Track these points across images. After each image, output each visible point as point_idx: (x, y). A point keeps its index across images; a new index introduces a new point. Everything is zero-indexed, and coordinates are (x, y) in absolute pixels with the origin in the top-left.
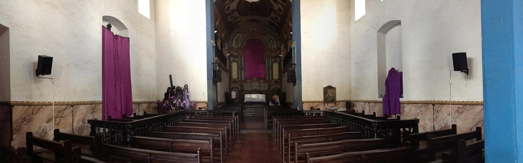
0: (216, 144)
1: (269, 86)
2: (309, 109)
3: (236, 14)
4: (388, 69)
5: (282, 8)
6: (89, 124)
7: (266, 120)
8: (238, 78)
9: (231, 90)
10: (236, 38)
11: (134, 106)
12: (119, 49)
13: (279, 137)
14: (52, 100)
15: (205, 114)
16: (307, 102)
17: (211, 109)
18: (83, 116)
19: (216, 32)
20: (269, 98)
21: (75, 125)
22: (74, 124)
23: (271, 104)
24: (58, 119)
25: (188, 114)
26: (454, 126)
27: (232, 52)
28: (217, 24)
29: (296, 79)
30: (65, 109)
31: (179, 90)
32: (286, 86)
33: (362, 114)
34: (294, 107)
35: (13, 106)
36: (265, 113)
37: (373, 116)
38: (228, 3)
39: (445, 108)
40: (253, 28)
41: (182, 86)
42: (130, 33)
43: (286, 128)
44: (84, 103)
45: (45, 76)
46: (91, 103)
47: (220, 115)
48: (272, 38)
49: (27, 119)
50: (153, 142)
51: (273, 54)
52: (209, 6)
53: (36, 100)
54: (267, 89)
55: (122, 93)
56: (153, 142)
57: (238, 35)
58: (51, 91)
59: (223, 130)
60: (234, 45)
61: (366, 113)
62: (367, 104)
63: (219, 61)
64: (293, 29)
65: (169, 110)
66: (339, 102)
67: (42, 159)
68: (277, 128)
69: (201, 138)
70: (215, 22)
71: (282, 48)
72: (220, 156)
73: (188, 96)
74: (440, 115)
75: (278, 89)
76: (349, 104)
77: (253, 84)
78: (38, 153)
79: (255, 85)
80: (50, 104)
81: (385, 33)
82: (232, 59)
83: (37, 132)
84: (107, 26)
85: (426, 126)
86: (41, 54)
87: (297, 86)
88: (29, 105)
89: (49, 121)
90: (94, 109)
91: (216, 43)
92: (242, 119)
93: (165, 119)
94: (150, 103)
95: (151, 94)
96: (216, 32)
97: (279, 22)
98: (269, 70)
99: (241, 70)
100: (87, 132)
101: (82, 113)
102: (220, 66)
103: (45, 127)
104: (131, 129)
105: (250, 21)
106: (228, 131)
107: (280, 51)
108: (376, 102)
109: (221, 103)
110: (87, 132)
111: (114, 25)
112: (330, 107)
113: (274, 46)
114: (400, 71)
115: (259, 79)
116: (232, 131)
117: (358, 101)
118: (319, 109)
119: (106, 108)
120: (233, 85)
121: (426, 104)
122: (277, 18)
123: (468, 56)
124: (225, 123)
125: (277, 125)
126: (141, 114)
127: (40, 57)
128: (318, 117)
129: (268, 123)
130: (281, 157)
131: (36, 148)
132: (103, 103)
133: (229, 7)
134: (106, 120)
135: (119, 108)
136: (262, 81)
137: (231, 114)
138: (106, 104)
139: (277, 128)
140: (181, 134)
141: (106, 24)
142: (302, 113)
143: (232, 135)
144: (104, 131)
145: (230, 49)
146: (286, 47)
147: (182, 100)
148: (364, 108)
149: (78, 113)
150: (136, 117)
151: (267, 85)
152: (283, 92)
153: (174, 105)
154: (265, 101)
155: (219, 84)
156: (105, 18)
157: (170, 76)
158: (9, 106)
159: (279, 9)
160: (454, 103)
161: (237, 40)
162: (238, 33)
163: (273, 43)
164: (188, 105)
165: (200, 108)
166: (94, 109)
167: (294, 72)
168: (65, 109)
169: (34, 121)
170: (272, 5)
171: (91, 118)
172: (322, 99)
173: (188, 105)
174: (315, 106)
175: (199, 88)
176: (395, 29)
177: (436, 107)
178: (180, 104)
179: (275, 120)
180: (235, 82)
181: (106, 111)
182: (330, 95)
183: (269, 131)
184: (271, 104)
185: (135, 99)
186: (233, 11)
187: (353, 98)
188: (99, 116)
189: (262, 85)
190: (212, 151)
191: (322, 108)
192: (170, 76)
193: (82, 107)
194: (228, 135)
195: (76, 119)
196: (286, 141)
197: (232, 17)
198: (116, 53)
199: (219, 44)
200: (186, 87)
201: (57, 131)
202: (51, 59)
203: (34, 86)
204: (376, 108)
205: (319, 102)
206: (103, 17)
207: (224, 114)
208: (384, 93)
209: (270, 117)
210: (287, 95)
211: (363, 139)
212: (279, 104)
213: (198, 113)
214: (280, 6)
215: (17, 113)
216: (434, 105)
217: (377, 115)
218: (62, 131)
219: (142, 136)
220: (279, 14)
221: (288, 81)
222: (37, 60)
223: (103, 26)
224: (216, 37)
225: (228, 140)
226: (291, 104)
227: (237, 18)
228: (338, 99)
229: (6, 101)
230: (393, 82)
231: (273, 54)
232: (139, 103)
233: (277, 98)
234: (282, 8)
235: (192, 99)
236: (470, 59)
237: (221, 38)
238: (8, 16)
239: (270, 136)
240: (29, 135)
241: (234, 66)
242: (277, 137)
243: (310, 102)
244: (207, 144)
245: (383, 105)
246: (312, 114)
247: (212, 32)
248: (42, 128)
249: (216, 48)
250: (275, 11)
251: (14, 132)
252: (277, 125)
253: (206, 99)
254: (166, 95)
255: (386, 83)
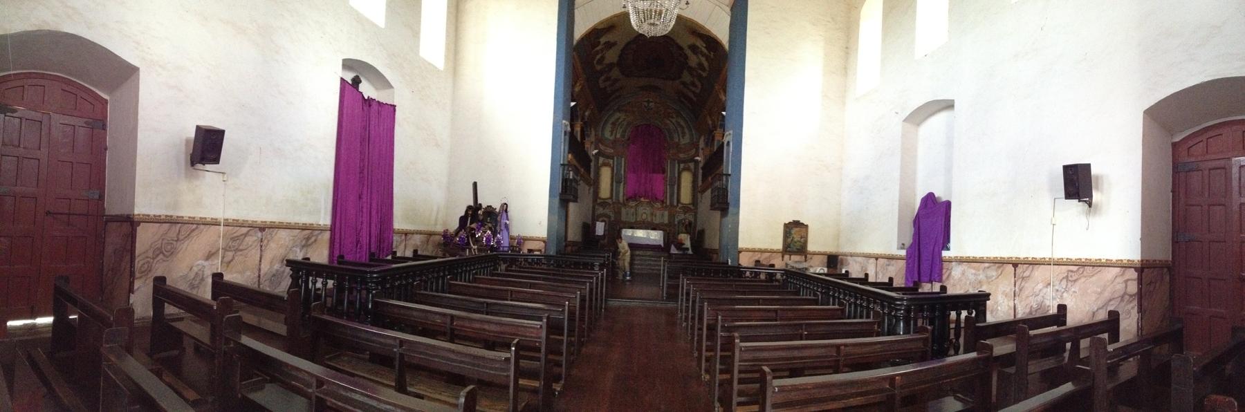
0: (554, 327)
1: (672, 216)
2: (752, 265)
3: (615, 73)
4: (921, 194)
5: (706, 64)
6: (288, 269)
7: (665, 281)
8: (611, 197)
9: (595, 219)
10: (612, 120)
11: (396, 238)
12: (372, 127)
13: (693, 318)
14: (219, 214)
15: (539, 262)
16: (748, 250)
17: (552, 252)
18: (282, 251)
19: (573, 104)
20: (670, 239)
21: (265, 267)
22: (258, 268)
23: (674, 250)
24: (230, 254)
25: (505, 261)
26: (1062, 308)
27: (602, 147)
28: (577, 89)
29: (728, 204)
30: (246, 235)
31: (490, 212)
32: (709, 219)
33: (864, 280)
34: (721, 259)
35: (139, 223)
36: (662, 265)
37: (889, 285)
38: (602, 50)
39: (1039, 272)
40: (648, 102)
41: (497, 206)
42: (401, 97)
43: (710, 301)
44: (288, 227)
45: (208, 167)
46: (304, 228)
47: (569, 266)
48: (682, 123)
49: (166, 251)
50: (415, 313)
51: (682, 156)
52: (563, 55)
53: (186, 212)
54: (666, 220)
55: (374, 213)
56: (415, 313)
57: (617, 115)
58: (214, 197)
59: (573, 298)
60: (607, 134)
61: (871, 279)
62: (873, 260)
63: (575, 162)
64: (729, 104)
65: (464, 250)
66: (814, 254)
67: (180, 334)
68: (688, 300)
69: (518, 312)
70: (573, 86)
71: (702, 144)
72: (539, 350)
73: (507, 226)
74: (1028, 286)
75: (690, 223)
76: (833, 260)
77: (641, 210)
78: (174, 320)
79: (644, 212)
80: (215, 223)
81: (918, 125)
82: (601, 160)
83: (184, 277)
84: (353, 80)
85: (999, 310)
86: (203, 123)
87: (729, 218)
88: (172, 221)
89: (210, 256)
90: (308, 239)
91: (572, 126)
92: (614, 281)
93: (452, 268)
94: (430, 234)
95: (433, 218)
96: (573, 104)
97: (698, 91)
98: (672, 186)
99: (619, 182)
100: (282, 287)
101: (281, 247)
102: (577, 171)
103: (192, 268)
104: (377, 284)
105: (642, 88)
106: (583, 300)
107: (697, 149)
108: (891, 258)
109: (574, 243)
110: (282, 287)
111: (368, 80)
112: (794, 261)
113: (685, 140)
114: (944, 199)
115: (653, 199)
116: (591, 300)
117: (852, 255)
118: (773, 266)
119: (337, 240)
120: (600, 211)
121: (1000, 263)
122: (693, 84)
123: (1094, 171)
124: (577, 283)
125: (688, 294)
126: (409, 254)
127: (198, 128)
128: (772, 281)
129: (669, 287)
130: (694, 364)
131: (170, 310)
132: (333, 229)
133: (603, 58)
134: (336, 264)
135: (365, 241)
136: (658, 205)
137: (593, 266)
138: (337, 230)
139: (688, 300)
140: (482, 303)
141: (349, 77)
142: (738, 271)
143: (590, 308)
144: (325, 284)
145: (599, 141)
146: (710, 140)
147: (495, 233)
148: (863, 268)
149: (273, 245)
150: (397, 260)
151: (666, 213)
152: (699, 228)
153: (477, 241)
154: (662, 243)
155: (572, 206)
156: (348, 64)
157: (475, 184)
158: (130, 223)
159: (700, 65)
160: (1059, 263)
161: (613, 124)
162: (619, 110)
163: (684, 134)
164: (505, 243)
165: (530, 251)
166: (308, 239)
167: (726, 190)
168: (246, 235)
169: (179, 255)
170: (686, 58)
171: (299, 256)
172: (779, 245)
173: (505, 243)
174: (763, 258)
175: (532, 214)
176: (942, 117)
177: (1020, 269)
178: (488, 240)
179: (684, 282)
180: (604, 204)
181: (337, 246)
182: (797, 238)
183: (671, 305)
184: (674, 250)
185: (398, 224)
186: (611, 66)
187: (845, 249)
188: (320, 255)
189: (658, 213)
190: (544, 342)
191: (779, 263)
192: (475, 184)
193: (283, 234)
194: (582, 307)
195: (268, 256)
196: (712, 328)
197: (608, 79)
198: (366, 131)
199: (578, 129)
200: (505, 208)
201: (217, 277)
202: (221, 133)
203: (184, 186)
204: (890, 268)
205: (772, 251)
206: (344, 61)
207: (577, 264)
208: (908, 241)
209: (673, 276)
210: (707, 232)
211: (878, 335)
212: (690, 252)
213: (526, 260)
214: (703, 59)
215: (145, 238)
216: (1015, 265)
217: (895, 285)
218: (228, 277)
219: (400, 300)
220: (700, 76)
221: (713, 207)
222: (192, 135)
223: (342, 79)
224: (573, 115)
225: (582, 319)
226: (715, 251)
227: (617, 80)
228: (811, 247)
229: (125, 212)
230: (932, 221)
231: (682, 156)
232: (406, 233)
233: (686, 239)
234: (706, 64)
235: (515, 232)
236: (1097, 178)
237: (583, 119)
238: (138, 43)
239: (671, 314)
240: (160, 281)
241: (606, 175)
242: (687, 318)
243: (754, 251)
244: (536, 328)
245: (908, 264)
246: (757, 274)
247: (566, 103)
248: (195, 269)
249: (571, 136)
250: (690, 69)
251: (137, 275)
252: (688, 294)
253: (542, 232)
254: (463, 220)
255: (915, 222)
